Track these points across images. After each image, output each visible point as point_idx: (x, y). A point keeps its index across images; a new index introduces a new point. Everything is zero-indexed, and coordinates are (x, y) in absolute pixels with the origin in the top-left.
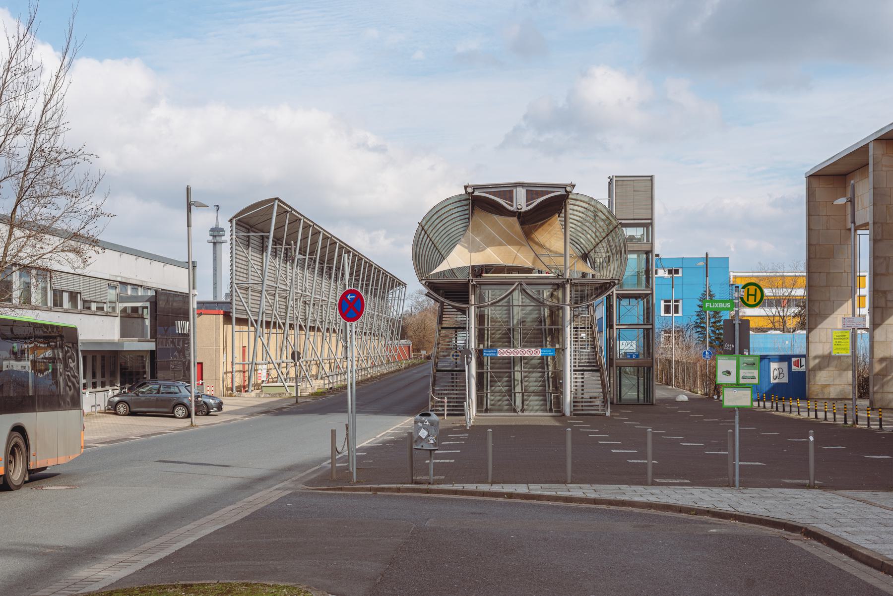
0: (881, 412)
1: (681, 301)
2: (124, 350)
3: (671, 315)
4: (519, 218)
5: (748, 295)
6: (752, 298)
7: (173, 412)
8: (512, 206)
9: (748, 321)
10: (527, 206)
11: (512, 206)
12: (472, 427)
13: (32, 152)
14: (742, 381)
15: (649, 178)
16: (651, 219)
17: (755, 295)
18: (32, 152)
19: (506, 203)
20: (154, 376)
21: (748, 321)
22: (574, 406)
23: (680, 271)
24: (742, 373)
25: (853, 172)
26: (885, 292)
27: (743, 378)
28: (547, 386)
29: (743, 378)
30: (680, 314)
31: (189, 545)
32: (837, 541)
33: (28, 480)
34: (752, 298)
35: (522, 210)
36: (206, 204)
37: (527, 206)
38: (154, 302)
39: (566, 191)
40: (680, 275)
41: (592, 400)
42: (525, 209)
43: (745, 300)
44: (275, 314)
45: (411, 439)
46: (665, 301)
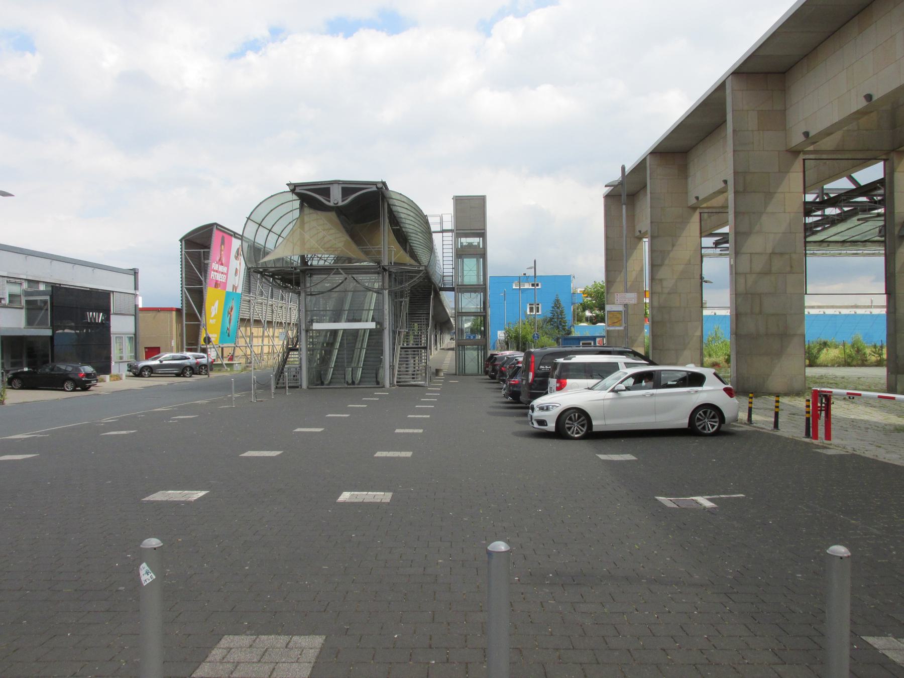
0: (751, 398)
1: (540, 304)
2: (752, 415)
3: (534, 313)
4: (337, 213)
7: (63, 386)
8: (329, 201)
11: (329, 201)
13: (333, 289)
15: (483, 198)
16: (484, 229)
18: (333, 289)
19: (325, 199)
20: (53, 361)
23: (539, 285)
26: (661, 280)
30: (540, 313)
31: (825, 421)
32: (178, 500)
33: (553, 430)
35: (338, 205)
36: (10, 192)
39: (377, 187)
40: (539, 287)
41: (407, 356)
42: (341, 204)
44: (614, 367)
46: (530, 305)
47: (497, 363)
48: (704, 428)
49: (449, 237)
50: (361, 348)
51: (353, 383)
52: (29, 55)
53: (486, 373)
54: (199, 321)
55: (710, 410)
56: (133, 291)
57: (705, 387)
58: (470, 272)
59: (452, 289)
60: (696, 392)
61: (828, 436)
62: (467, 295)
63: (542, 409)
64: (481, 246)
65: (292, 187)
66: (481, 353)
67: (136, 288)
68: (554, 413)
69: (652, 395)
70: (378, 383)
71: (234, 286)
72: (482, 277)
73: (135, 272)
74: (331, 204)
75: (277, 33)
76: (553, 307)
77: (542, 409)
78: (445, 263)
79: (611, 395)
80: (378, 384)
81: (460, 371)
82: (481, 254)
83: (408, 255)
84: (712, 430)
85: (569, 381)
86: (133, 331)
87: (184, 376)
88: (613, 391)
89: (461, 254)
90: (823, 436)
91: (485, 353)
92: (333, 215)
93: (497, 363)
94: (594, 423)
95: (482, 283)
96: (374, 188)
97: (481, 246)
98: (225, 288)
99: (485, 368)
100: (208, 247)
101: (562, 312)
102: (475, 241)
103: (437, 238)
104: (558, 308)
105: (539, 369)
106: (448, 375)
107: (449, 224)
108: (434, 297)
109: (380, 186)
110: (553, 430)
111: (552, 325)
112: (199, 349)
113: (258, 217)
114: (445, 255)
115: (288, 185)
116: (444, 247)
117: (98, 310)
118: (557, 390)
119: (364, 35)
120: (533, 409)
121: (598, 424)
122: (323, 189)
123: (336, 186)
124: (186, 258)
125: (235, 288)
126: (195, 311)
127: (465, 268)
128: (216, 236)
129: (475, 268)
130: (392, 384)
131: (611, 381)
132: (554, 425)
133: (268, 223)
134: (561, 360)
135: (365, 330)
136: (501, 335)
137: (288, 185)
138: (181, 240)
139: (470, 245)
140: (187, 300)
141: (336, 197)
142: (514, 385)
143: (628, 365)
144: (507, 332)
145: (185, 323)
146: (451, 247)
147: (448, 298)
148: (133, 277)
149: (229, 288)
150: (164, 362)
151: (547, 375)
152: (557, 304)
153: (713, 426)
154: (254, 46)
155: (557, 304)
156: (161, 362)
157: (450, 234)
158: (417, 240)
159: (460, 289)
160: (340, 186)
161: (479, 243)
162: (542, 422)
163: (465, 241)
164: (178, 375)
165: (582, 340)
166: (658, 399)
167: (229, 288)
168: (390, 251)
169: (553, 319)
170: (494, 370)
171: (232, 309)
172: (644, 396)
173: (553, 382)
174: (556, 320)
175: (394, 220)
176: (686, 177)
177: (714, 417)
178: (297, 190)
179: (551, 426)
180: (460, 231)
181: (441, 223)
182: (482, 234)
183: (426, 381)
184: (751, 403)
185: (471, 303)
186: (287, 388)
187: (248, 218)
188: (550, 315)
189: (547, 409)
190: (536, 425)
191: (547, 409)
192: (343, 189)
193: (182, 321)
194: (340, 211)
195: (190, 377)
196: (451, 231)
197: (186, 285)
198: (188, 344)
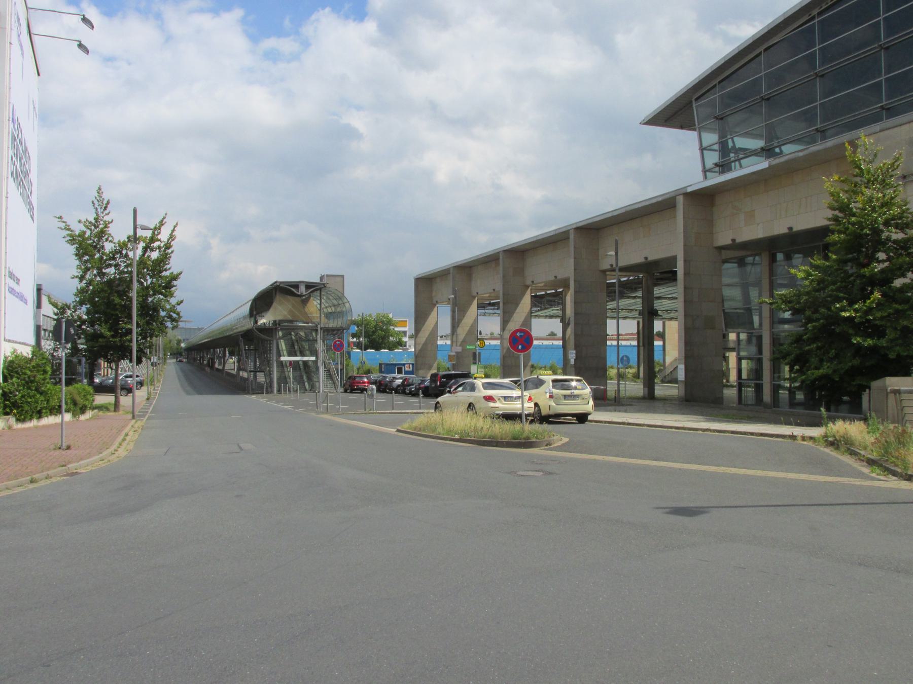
10: (306, 292)
37: (306, 292)
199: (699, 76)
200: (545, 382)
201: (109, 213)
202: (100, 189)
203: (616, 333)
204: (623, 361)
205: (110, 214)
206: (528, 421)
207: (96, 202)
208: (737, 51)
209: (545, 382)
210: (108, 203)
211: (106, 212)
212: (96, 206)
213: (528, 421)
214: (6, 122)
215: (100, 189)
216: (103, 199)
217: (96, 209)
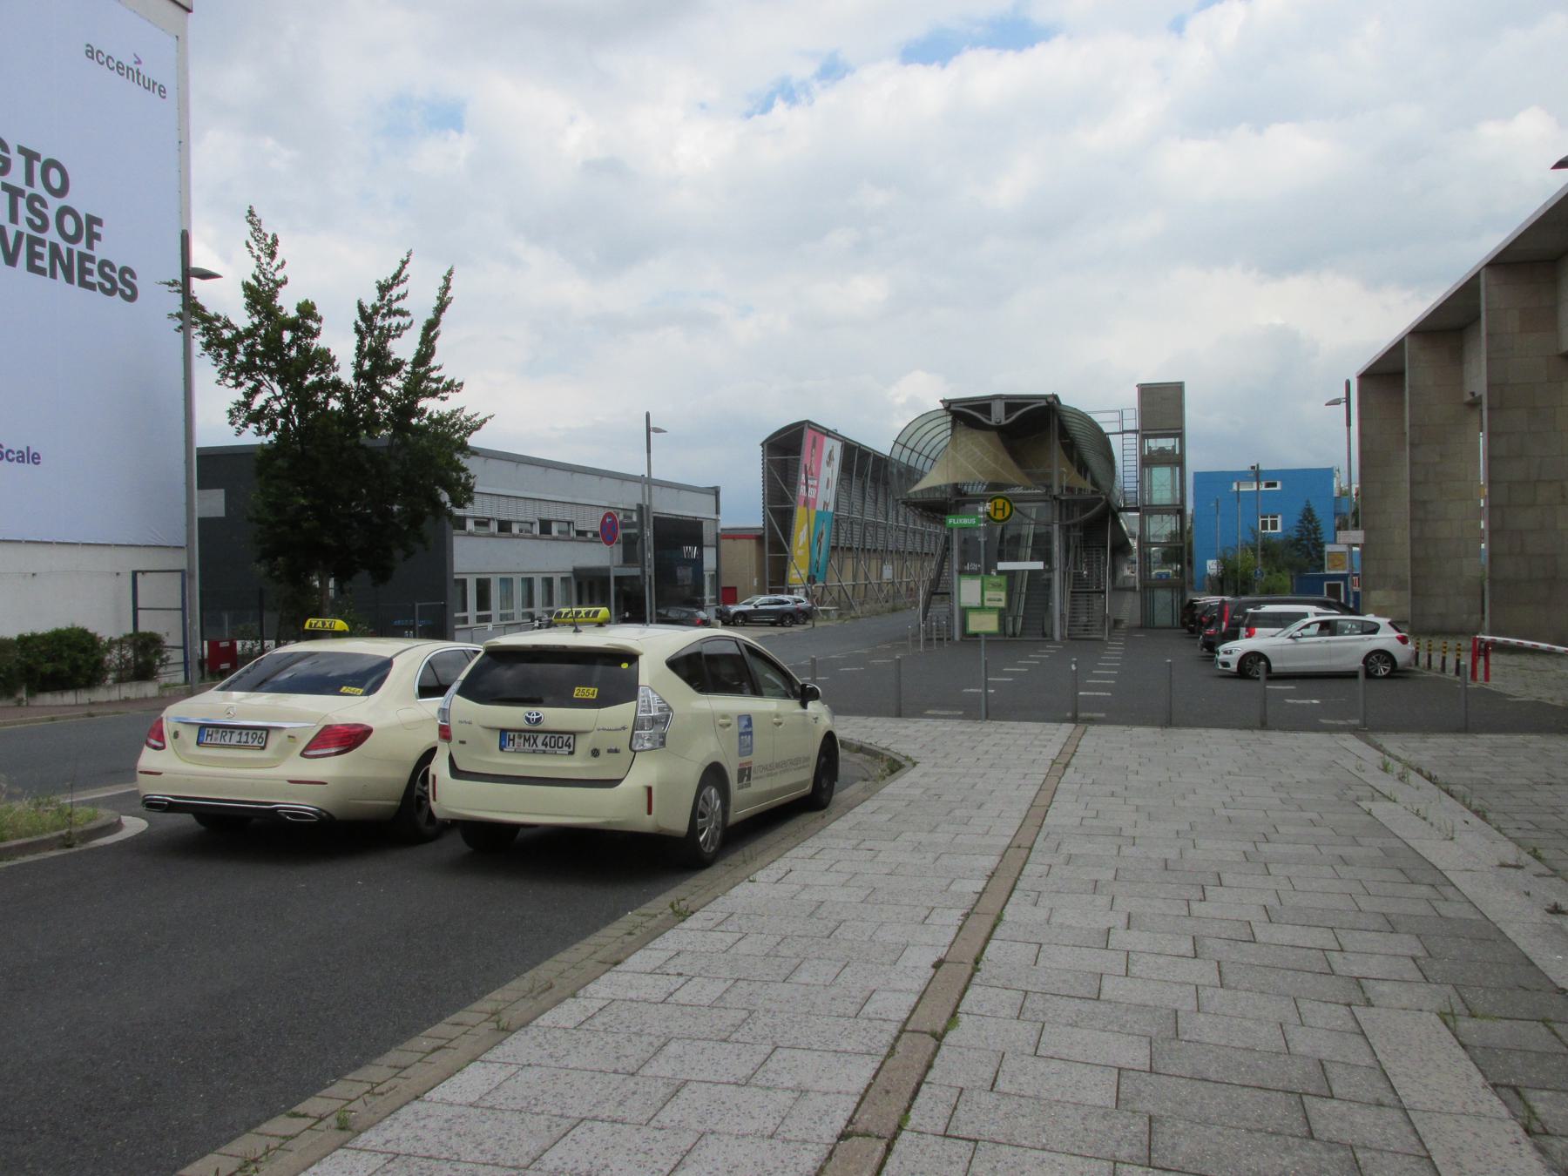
5: (995, 509)
6: (999, 513)
9: (203, 522)
10: (1006, 419)
12: (468, 843)
14: (987, 604)
17: (1003, 509)
21: (203, 522)
22: (506, 583)
24: (987, 594)
25: (145, 546)
26: (1424, 502)
27: (989, 600)
28: (654, 607)
29: (989, 600)
30: (1279, 530)
34: (999, 513)
36: (662, 428)
37: (1006, 419)
38: (611, 543)
40: (1279, 487)
42: (1004, 422)
43: (992, 514)
44: (1305, 615)
45: (278, 645)
47: (1196, 612)
48: (1377, 671)
49: (1132, 440)
50: (1020, 593)
51: (1014, 635)
52: (454, 135)
53: (1184, 625)
54: (786, 552)
55: (1383, 655)
56: (714, 517)
57: (1379, 635)
58: (1162, 484)
59: (1136, 510)
60: (1370, 639)
61: (1487, 678)
62: (1157, 518)
63: (1226, 653)
64: (1177, 452)
65: (947, 404)
66: (1177, 598)
67: (717, 512)
68: (1236, 656)
69: (1328, 641)
70: (1044, 635)
71: (825, 503)
72: (1178, 492)
73: (716, 492)
74: (992, 423)
75: (832, 70)
76: (1301, 521)
77: (1226, 653)
78: (1126, 469)
79: (1290, 641)
80: (1046, 635)
81: (1147, 624)
82: (1176, 460)
83: (1075, 469)
84: (1384, 673)
85: (1258, 630)
86: (714, 566)
87: (783, 626)
88: (1291, 637)
89: (1149, 461)
90: (1483, 678)
91: (1182, 600)
92: (993, 435)
93: (1196, 612)
94: (1273, 665)
95: (1178, 502)
96: (1043, 403)
97: (1177, 452)
98: (814, 507)
99: (1182, 618)
100: (798, 452)
101: (1316, 529)
102: (1168, 443)
103: (1115, 442)
104: (1310, 522)
105: (1233, 619)
106: (1131, 629)
107: (1132, 422)
108: (1112, 524)
109: (1050, 400)
110: (1235, 670)
111: (1299, 550)
112: (786, 590)
113: (902, 440)
114: (1126, 469)
115: (941, 401)
116: (1125, 442)
117: (693, 545)
118: (1357, 672)
119: (971, 59)
120: (1218, 653)
121: (1276, 666)
122: (984, 405)
123: (998, 401)
124: (768, 468)
125: (826, 504)
126: (777, 534)
127: (1155, 481)
128: (808, 436)
129: (1168, 482)
130: (1062, 636)
131: (1293, 629)
132: (1236, 666)
133: (926, 452)
134: (1251, 610)
135: (1023, 571)
136: (1212, 566)
137: (941, 401)
138: (762, 445)
139: (1162, 450)
140: (769, 520)
141: (998, 415)
142: (1210, 636)
143: (1317, 614)
144: (1224, 562)
145: (767, 555)
146: (1134, 452)
147: (1129, 522)
148: (714, 498)
149: (820, 507)
150: (760, 607)
151: (1239, 624)
152: (1308, 516)
153: (1385, 670)
154: (789, 92)
155: (1308, 516)
156: (756, 606)
157: (1134, 436)
158: (1094, 461)
159: (1148, 510)
160: (1003, 402)
161: (1174, 447)
162: (1226, 664)
163: (1155, 444)
164: (773, 624)
165: (1329, 580)
166: (1332, 645)
167: (820, 507)
168: (1061, 474)
169: (1302, 540)
170: (1193, 621)
171: (822, 534)
172: (1319, 642)
173: (1243, 630)
174: (1305, 542)
175: (1064, 432)
176: (1461, 363)
177: (1386, 662)
178: (953, 408)
179: (1234, 667)
180: (1145, 432)
181: (1121, 421)
182: (1179, 434)
183: (1104, 634)
184: (1459, 655)
185: (1163, 527)
186: (935, 642)
187: (896, 442)
188: (1294, 534)
189: (1231, 652)
190: (1220, 667)
191: (1231, 652)
192: (1007, 405)
193: (764, 552)
194: (1000, 429)
195: (804, 624)
196: (1135, 432)
197: (769, 503)
198: (771, 583)
199: (1545, 204)
200: (1178, 388)
201: (283, 263)
202: (251, 213)
203: (182, 660)
204: (648, 527)
205: (285, 266)
206: (427, 415)
207: (253, 243)
208: (1543, 212)
209: (1178, 388)
210: (275, 241)
211: (277, 262)
212: (257, 252)
213: (427, 415)
214: (1298, 647)
215: (251, 213)
216: (265, 234)
217: (258, 258)
